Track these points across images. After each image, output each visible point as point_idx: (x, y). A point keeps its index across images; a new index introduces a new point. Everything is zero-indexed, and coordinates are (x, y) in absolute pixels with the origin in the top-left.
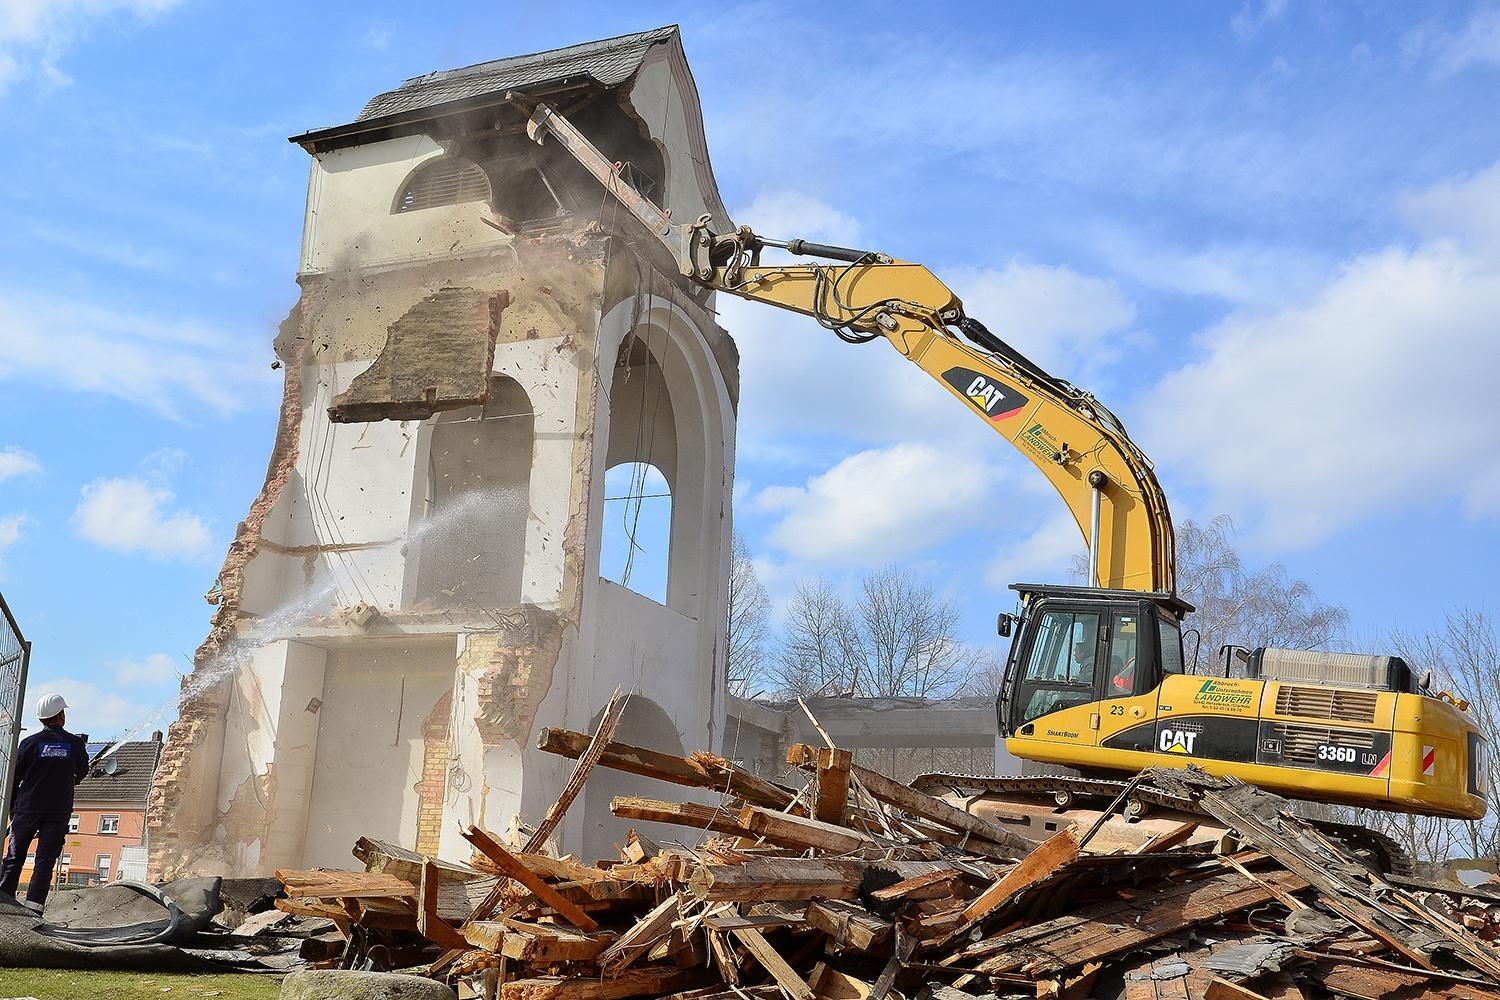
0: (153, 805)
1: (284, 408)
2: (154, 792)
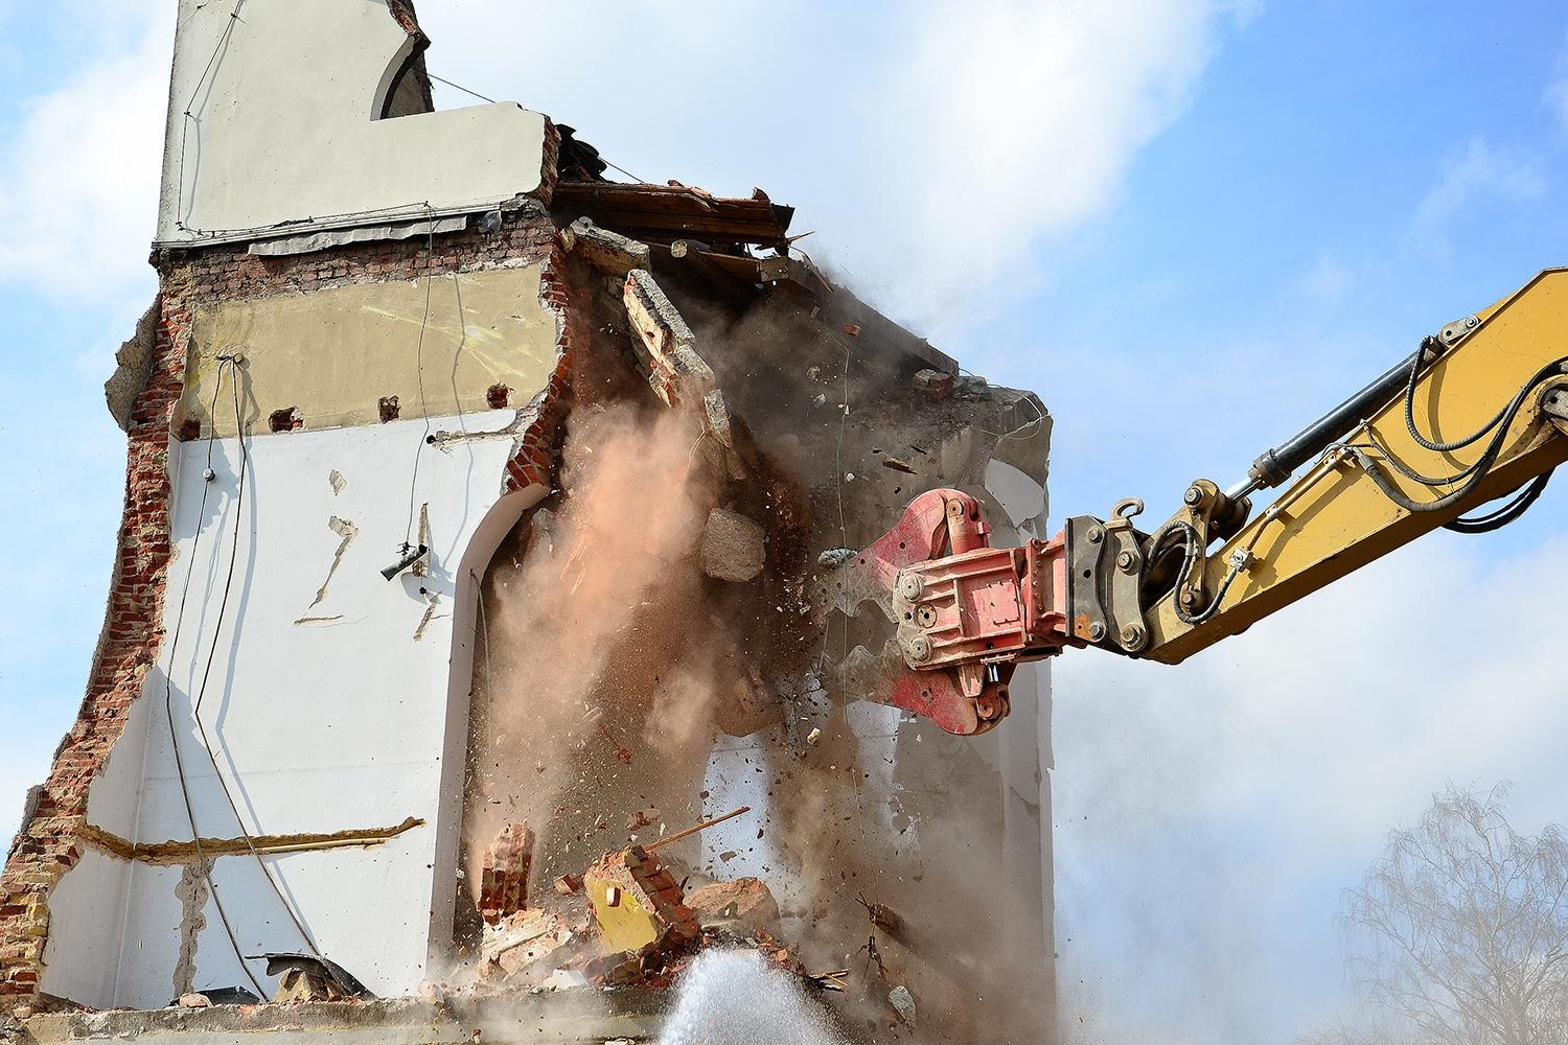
1: (126, 533)
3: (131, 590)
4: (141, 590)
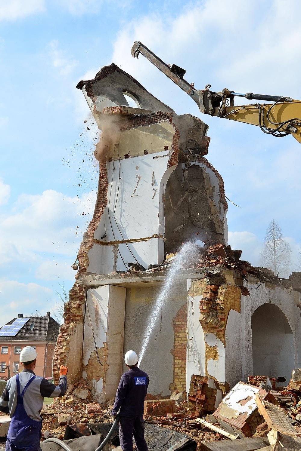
0: (55, 363)
1: (100, 181)
2: (55, 357)
3: (102, 192)
4: (103, 192)
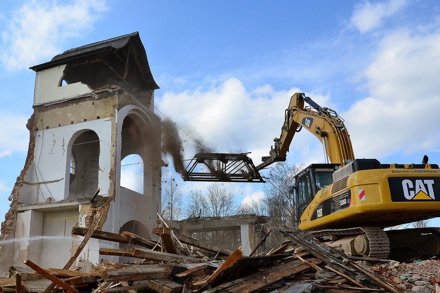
1: (30, 144)
